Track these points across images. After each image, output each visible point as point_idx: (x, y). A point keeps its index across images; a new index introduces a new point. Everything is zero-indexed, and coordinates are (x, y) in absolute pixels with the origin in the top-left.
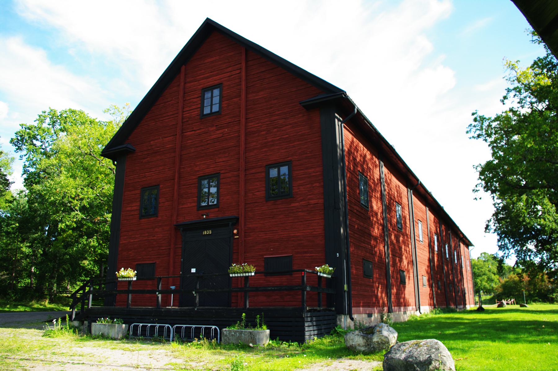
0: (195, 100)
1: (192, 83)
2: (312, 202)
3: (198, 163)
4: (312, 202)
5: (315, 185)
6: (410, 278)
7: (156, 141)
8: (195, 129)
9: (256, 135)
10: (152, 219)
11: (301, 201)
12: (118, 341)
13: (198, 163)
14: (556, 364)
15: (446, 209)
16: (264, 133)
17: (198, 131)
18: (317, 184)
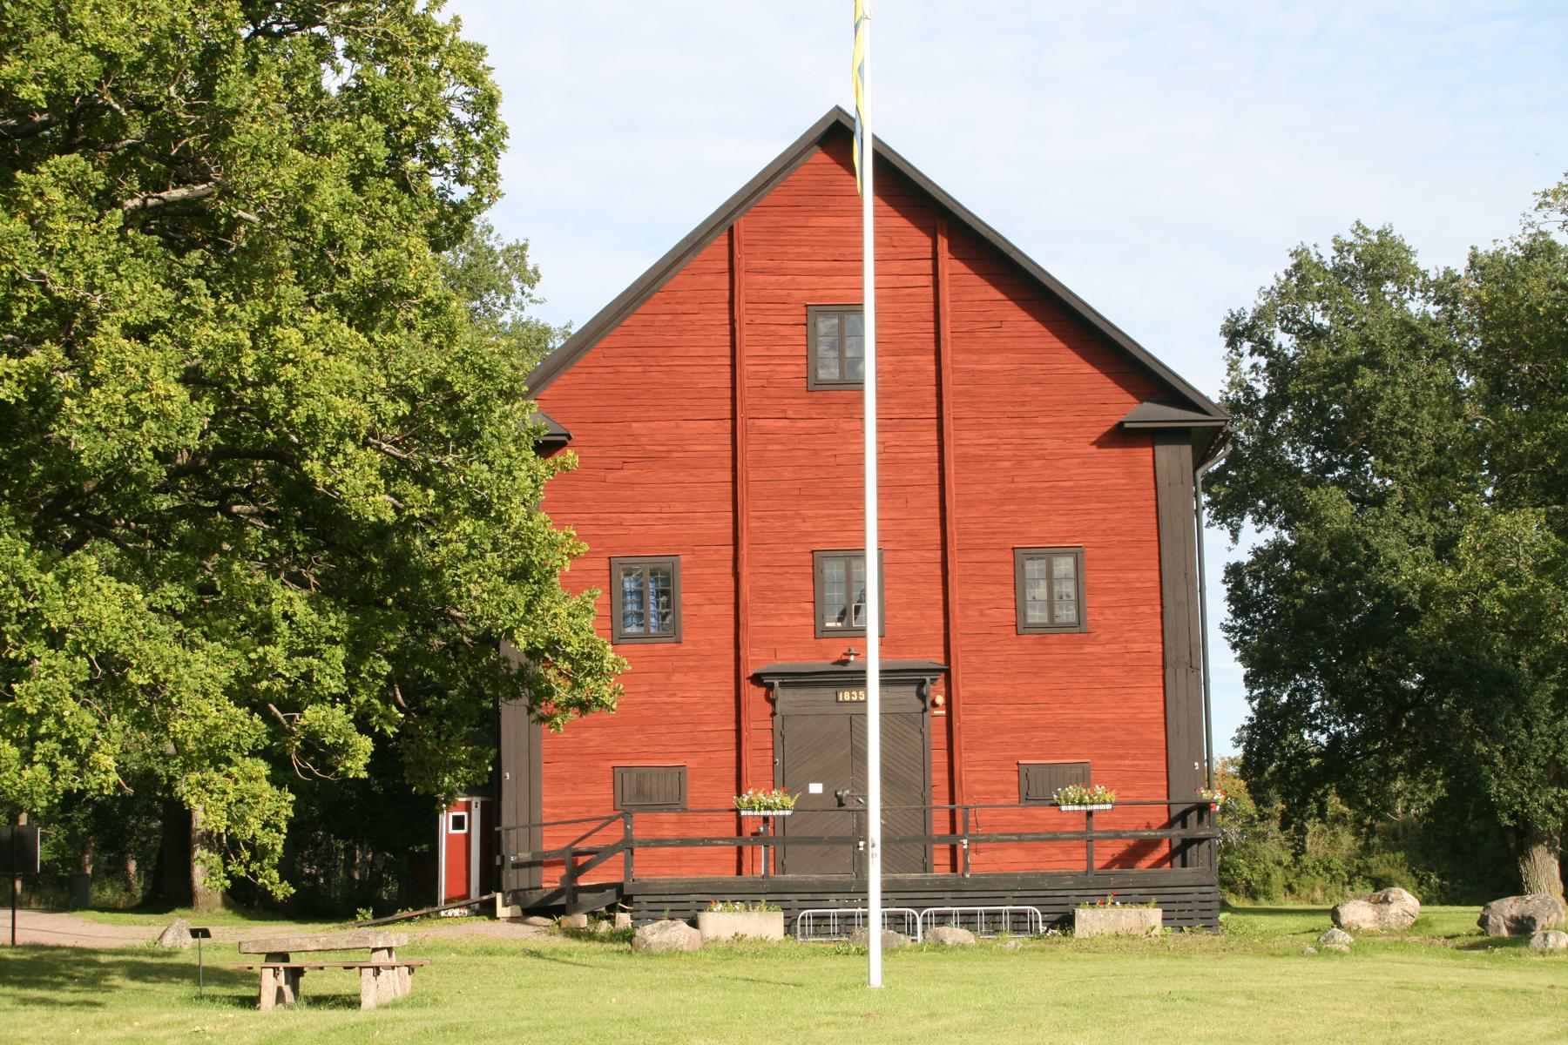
0: (786, 331)
1: (773, 278)
2: (1136, 647)
3: (809, 513)
4: (1136, 647)
5: (1141, 609)
6: (687, 599)
7: (652, 425)
8: (790, 414)
9: (986, 466)
10: (658, 647)
11: (1109, 642)
12: (596, 945)
13: (809, 513)
14: (1563, 286)
15: (1144, 345)
16: (1007, 464)
17: (802, 424)
18: (1147, 609)
